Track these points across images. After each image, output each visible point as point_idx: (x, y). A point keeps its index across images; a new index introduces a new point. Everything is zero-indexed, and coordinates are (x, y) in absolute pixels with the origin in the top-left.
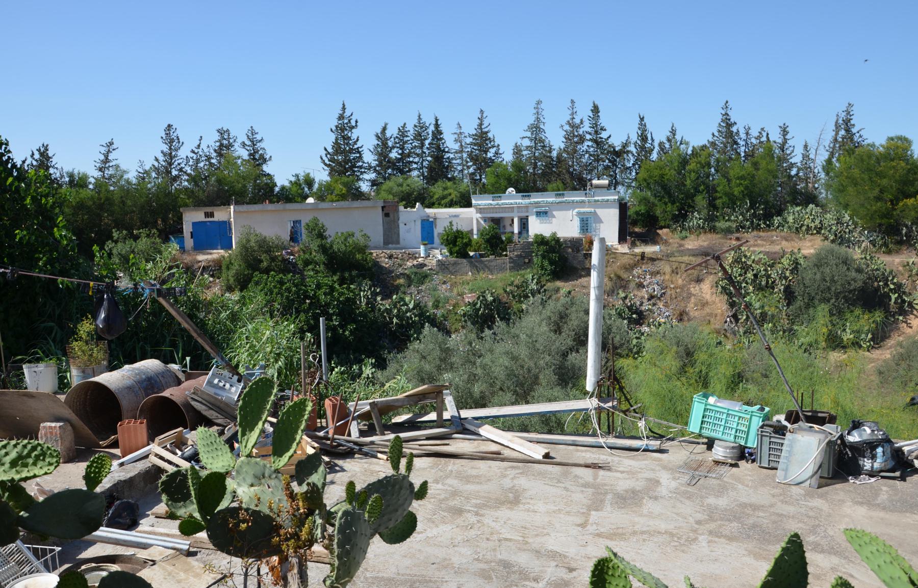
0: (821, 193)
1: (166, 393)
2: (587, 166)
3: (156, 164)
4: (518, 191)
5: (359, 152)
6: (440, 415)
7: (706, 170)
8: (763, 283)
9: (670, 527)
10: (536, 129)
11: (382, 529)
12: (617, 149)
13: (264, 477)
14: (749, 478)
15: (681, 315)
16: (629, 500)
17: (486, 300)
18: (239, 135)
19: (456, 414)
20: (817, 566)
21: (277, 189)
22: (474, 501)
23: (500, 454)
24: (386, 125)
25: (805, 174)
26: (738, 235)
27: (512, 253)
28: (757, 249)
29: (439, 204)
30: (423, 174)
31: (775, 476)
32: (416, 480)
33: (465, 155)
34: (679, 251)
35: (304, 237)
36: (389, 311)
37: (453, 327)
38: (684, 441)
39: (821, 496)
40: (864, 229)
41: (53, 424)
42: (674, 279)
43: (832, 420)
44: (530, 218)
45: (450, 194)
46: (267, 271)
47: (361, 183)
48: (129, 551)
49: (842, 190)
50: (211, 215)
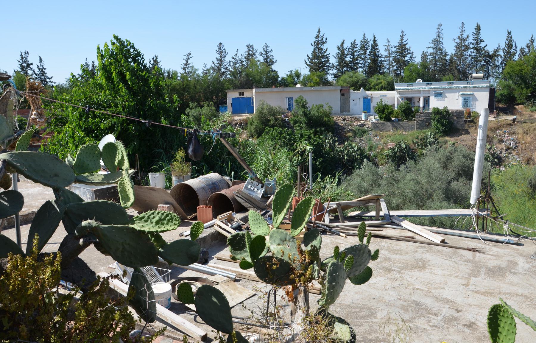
1: (223, 192)
2: (469, 65)
3: (213, 65)
5: (327, 57)
6: (378, 213)
9: (526, 292)
10: (437, 42)
11: (352, 276)
12: (490, 54)
13: (286, 240)
16: (496, 272)
18: (259, 48)
19: (387, 213)
21: (279, 79)
22: (397, 265)
23: (413, 238)
24: (344, 41)
27: (418, 119)
29: (374, 89)
30: (365, 71)
32: (372, 248)
33: (391, 59)
35: (294, 107)
36: (342, 152)
37: (380, 163)
41: (164, 206)
42: (525, 137)
44: (430, 98)
45: (381, 83)
46: (273, 126)
47: (328, 76)
48: (204, 276)
50: (242, 94)
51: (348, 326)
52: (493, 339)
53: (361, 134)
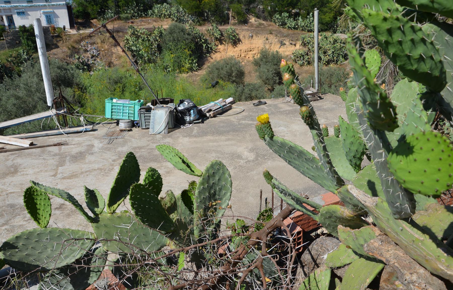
9: (100, 166)
14: (137, 135)
16: (78, 157)
20: (168, 168)
23: (3, 148)
28: (142, 27)
31: (149, 132)
38: (105, 124)
39: (169, 137)
40: (189, 14)
42: (103, 46)
43: (172, 101)
52: (33, 217)
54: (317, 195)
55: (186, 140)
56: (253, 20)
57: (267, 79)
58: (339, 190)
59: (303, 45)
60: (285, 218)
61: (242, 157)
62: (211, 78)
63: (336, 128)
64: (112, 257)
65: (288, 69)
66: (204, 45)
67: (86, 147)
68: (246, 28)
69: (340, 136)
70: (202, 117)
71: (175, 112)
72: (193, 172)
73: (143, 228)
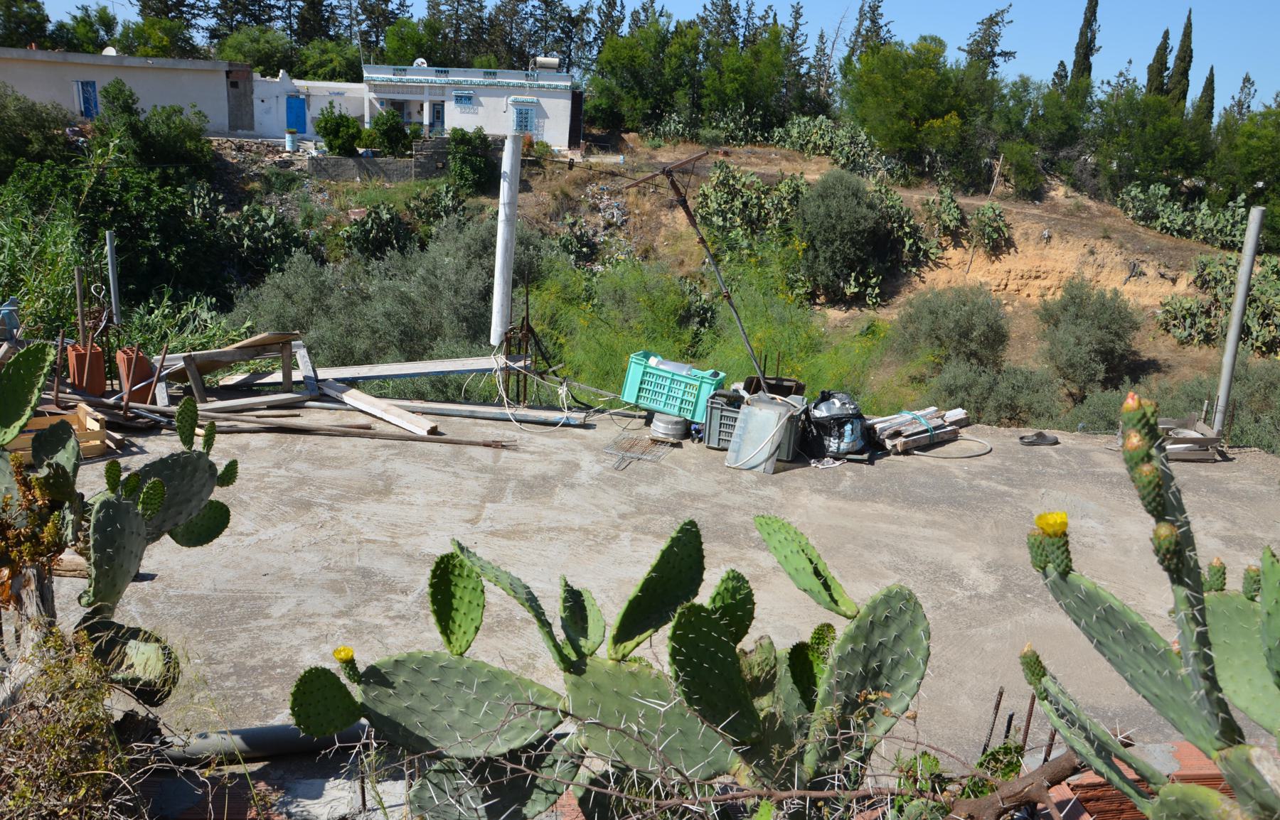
0: (835, 101)
2: (531, 36)
4: (431, 63)
6: (287, 375)
7: (692, 55)
8: (755, 215)
9: (587, 522)
12: (574, 15)
15: (647, 251)
16: (537, 488)
17: (380, 218)
19: (312, 374)
20: (758, 566)
21: (50, 27)
22: (328, 491)
23: (369, 428)
25: (818, 74)
26: (726, 148)
27: (418, 154)
28: (750, 169)
29: (315, 74)
31: (724, 458)
32: (219, 460)
34: (648, 165)
35: (101, 108)
36: (237, 229)
37: (332, 255)
38: (616, 414)
39: (775, 483)
43: (799, 390)
44: (446, 105)
45: (331, 61)
46: (40, 158)
47: (194, 33)
49: (859, 100)
51: (157, 645)
53: (282, 184)
54: (1159, 736)
55: (819, 500)
56: (1059, 192)
57: (1072, 366)
58: (1224, 753)
59: (1199, 283)
60: (1055, 782)
61: (961, 581)
62: (911, 335)
63: (1252, 574)
64: (596, 765)
65: (1140, 421)
66: (908, 242)
67: (559, 466)
68: (1036, 211)
69: (1258, 599)
70: (872, 446)
71: (803, 422)
72: (836, 602)
73: (683, 715)
